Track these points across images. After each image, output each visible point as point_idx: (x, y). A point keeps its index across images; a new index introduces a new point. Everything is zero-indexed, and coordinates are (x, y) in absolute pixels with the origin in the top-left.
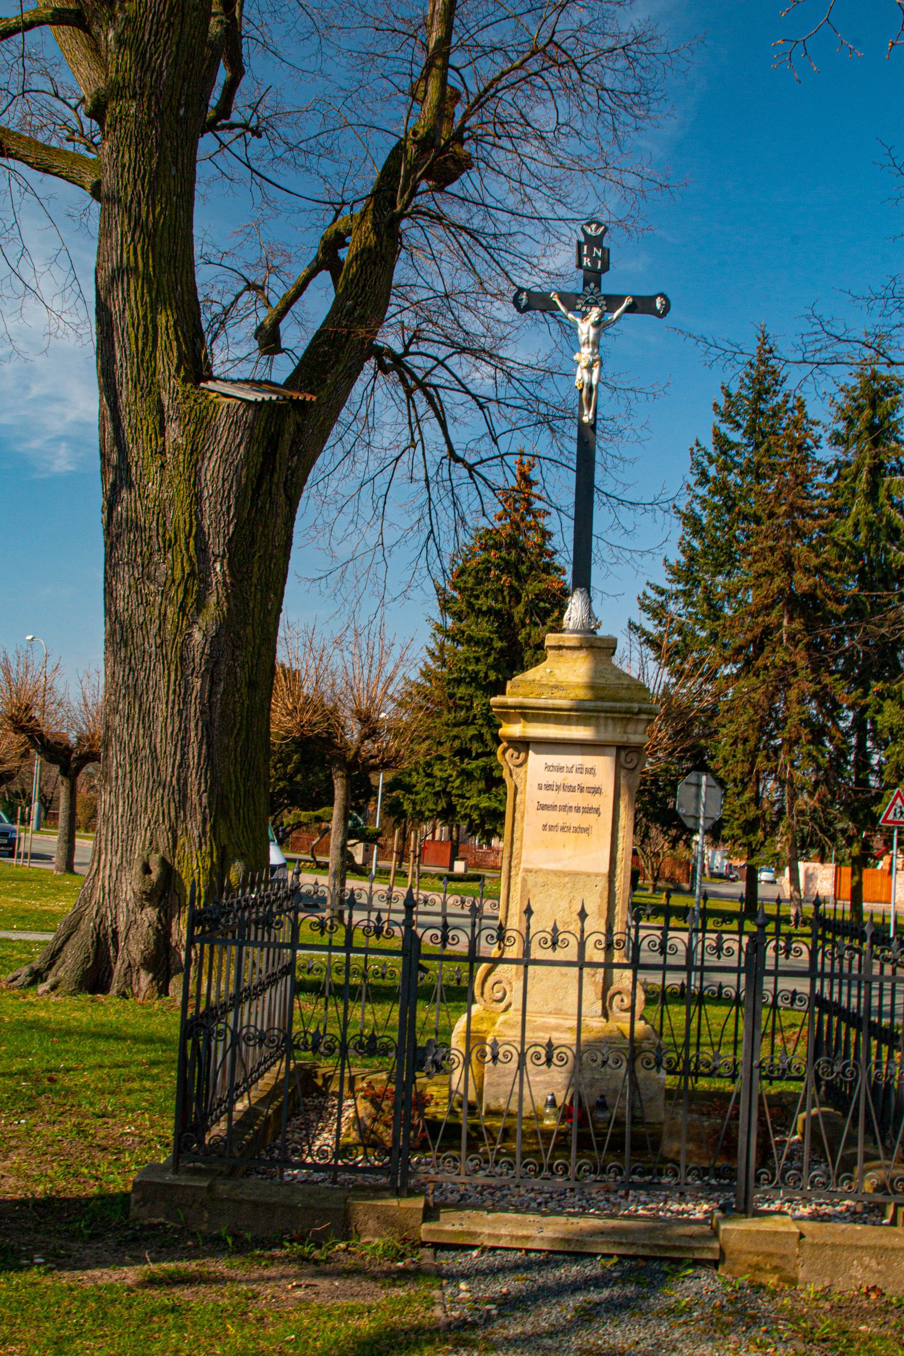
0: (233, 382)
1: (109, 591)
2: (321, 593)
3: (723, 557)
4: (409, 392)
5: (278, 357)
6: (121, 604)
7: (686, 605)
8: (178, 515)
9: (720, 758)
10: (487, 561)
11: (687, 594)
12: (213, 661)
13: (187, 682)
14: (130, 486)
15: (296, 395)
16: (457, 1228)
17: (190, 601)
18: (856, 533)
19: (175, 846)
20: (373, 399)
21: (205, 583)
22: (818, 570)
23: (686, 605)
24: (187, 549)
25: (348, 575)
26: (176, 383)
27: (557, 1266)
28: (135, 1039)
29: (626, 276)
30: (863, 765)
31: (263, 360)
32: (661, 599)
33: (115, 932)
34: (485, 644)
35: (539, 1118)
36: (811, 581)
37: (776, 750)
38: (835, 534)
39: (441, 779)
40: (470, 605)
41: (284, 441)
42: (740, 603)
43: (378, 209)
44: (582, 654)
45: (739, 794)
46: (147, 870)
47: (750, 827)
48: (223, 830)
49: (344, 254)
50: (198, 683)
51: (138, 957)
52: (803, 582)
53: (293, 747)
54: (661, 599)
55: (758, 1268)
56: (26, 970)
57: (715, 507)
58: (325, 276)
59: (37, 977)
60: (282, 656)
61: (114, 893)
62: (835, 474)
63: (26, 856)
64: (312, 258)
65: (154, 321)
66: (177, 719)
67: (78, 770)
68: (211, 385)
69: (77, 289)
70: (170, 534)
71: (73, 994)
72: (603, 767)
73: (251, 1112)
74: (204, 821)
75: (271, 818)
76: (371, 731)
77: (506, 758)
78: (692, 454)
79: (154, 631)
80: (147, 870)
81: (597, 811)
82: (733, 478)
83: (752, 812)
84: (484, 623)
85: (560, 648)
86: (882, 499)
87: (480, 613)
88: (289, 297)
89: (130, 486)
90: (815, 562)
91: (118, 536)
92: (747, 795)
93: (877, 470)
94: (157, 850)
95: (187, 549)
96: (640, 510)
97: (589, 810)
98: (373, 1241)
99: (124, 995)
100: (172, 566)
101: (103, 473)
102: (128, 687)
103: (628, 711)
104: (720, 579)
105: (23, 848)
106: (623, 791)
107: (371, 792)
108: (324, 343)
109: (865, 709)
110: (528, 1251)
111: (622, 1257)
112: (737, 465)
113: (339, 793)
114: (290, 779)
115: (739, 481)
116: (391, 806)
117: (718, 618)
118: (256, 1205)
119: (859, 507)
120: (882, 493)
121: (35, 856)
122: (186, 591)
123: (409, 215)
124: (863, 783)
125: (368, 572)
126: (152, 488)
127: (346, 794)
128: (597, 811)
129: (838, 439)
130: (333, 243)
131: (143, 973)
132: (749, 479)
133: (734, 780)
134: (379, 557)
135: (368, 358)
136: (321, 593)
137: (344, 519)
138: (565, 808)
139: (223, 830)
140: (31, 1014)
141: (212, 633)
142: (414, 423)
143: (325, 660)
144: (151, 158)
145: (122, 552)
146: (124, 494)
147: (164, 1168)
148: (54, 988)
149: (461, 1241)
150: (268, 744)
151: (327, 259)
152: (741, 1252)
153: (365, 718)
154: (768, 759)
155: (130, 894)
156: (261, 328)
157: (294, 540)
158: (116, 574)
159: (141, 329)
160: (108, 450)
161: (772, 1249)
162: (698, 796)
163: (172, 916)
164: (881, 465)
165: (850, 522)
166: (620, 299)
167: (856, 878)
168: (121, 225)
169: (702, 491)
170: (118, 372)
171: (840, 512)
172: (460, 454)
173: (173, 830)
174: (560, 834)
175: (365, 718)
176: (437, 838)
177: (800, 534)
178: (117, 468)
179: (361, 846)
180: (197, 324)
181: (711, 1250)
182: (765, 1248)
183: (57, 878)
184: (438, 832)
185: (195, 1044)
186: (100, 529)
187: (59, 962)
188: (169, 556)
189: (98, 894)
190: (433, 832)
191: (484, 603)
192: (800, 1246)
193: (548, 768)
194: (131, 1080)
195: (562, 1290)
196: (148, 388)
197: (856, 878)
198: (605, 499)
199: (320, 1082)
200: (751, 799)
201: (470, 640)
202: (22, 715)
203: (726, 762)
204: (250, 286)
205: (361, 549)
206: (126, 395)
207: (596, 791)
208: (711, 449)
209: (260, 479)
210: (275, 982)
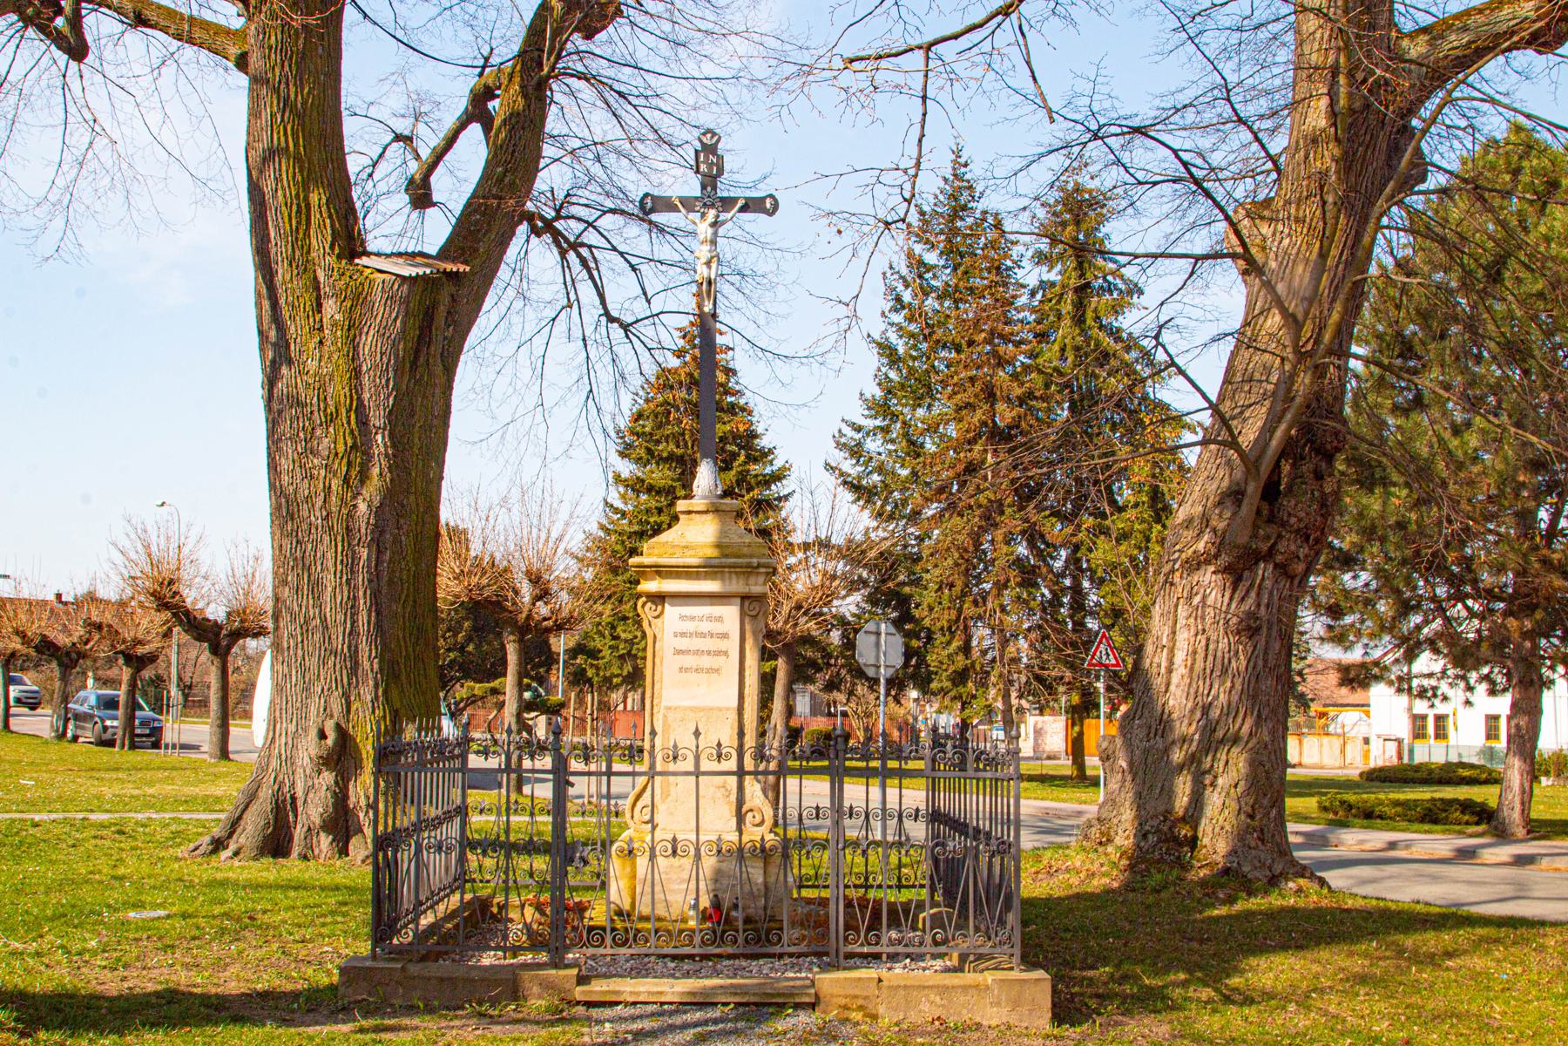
0: (388, 256)
1: (273, 466)
2: (482, 455)
3: (920, 388)
4: (563, 254)
5: (430, 211)
6: (286, 479)
7: (886, 441)
8: (338, 390)
9: (925, 606)
10: (666, 403)
11: (885, 430)
12: (379, 530)
13: (354, 552)
14: (290, 362)
15: (451, 267)
16: (605, 988)
17: (353, 474)
18: (1063, 358)
19: (349, 711)
20: (531, 261)
21: (368, 456)
22: (1022, 401)
23: (886, 441)
24: (349, 423)
25: (508, 436)
26: (331, 260)
27: (685, 1012)
28: (323, 888)
29: (739, 177)
30: (1078, 605)
31: (415, 214)
32: (858, 436)
33: (294, 798)
34: (668, 493)
35: (684, 920)
36: (1014, 413)
37: (984, 596)
38: (1040, 360)
39: (626, 641)
40: (649, 451)
41: (440, 308)
42: (941, 437)
43: (525, 70)
44: (710, 517)
45: (949, 643)
46: (322, 735)
47: (960, 677)
48: (395, 694)
49: (494, 105)
50: (364, 553)
51: (318, 821)
52: (1005, 414)
53: (463, 613)
54: (858, 436)
55: (846, 1008)
56: (207, 839)
57: (912, 336)
58: (475, 130)
59: (218, 845)
60: (446, 514)
61: (290, 760)
62: (1039, 296)
63: (174, 747)
64: (462, 109)
65: (306, 199)
66: (345, 589)
67: (229, 647)
68: (365, 261)
69: (222, 155)
70: (331, 409)
71: (255, 859)
72: (730, 615)
73: (433, 928)
74: (376, 686)
75: (442, 695)
76: (543, 594)
77: (647, 611)
78: (885, 277)
79: (319, 503)
80: (322, 735)
81: (726, 653)
82: (931, 303)
83: (961, 661)
84: (665, 467)
85: (689, 512)
86: (1090, 322)
87: (661, 460)
88: (439, 150)
89: (290, 362)
90: (1018, 391)
91: (280, 412)
92: (955, 644)
93: (1083, 290)
94: (332, 716)
95: (349, 423)
96: (795, 363)
97: (718, 653)
98: (537, 1003)
99: (305, 857)
100: (331, 441)
101: (262, 349)
102: (296, 559)
103: (749, 566)
104: (920, 412)
105: (168, 736)
106: (749, 636)
107: (550, 660)
108: (476, 211)
109: (1077, 548)
110: (662, 1004)
111: (738, 1004)
112: (933, 289)
113: (512, 658)
114: (462, 649)
115: (937, 306)
116: (575, 674)
117: (918, 455)
118: (442, 980)
119: (1065, 331)
120: (1089, 315)
121: (184, 747)
122: (349, 464)
123: (556, 77)
124: (1079, 625)
125: (528, 433)
126: (312, 365)
127: (519, 659)
128: (726, 653)
129: (1041, 258)
130: (481, 97)
131: (323, 835)
132: (947, 304)
133: (942, 629)
134: (539, 418)
135: (520, 223)
136: (482, 455)
137: (503, 381)
138: (698, 652)
139: (395, 694)
140: (219, 876)
141: (376, 503)
142: (570, 285)
143: (492, 521)
144: (297, 38)
145: (285, 428)
146: (284, 370)
147: (364, 959)
148: (236, 854)
149: (608, 998)
150: (435, 610)
151: (477, 110)
152: (832, 996)
153: (535, 579)
154: (976, 603)
155: (306, 760)
156: (411, 181)
157: (454, 409)
158: (279, 449)
159: (295, 208)
160: (266, 327)
161: (857, 992)
162: (878, 644)
163: (349, 780)
164: (1088, 285)
165: (1056, 347)
166: (736, 200)
167: (1077, 729)
168: (270, 106)
169: (898, 318)
170: (273, 251)
171: (1042, 337)
172: (614, 314)
173: (346, 695)
174: (694, 675)
175: (535, 579)
176: (629, 707)
177: (1001, 362)
178: (275, 345)
179: (543, 719)
180: (349, 202)
181: (808, 995)
182: (851, 992)
183: (211, 765)
184: (629, 701)
185: (385, 856)
186: (260, 406)
187: (239, 830)
188: (331, 430)
189: (274, 763)
190: (625, 701)
191: (665, 448)
192: (879, 989)
193: (682, 618)
194: (324, 916)
195: (685, 1026)
196: (305, 267)
197: (1077, 729)
198: (760, 354)
199: (495, 910)
200: (959, 648)
201: (650, 489)
202: (165, 591)
203: (931, 609)
204: (398, 138)
205: (521, 411)
206: (282, 272)
207: (725, 636)
208: (904, 271)
209: (417, 352)
210: (451, 818)
